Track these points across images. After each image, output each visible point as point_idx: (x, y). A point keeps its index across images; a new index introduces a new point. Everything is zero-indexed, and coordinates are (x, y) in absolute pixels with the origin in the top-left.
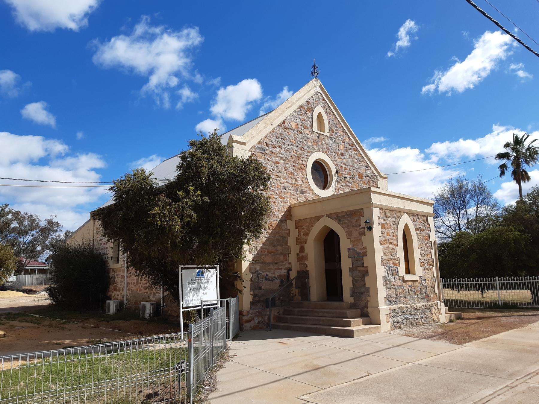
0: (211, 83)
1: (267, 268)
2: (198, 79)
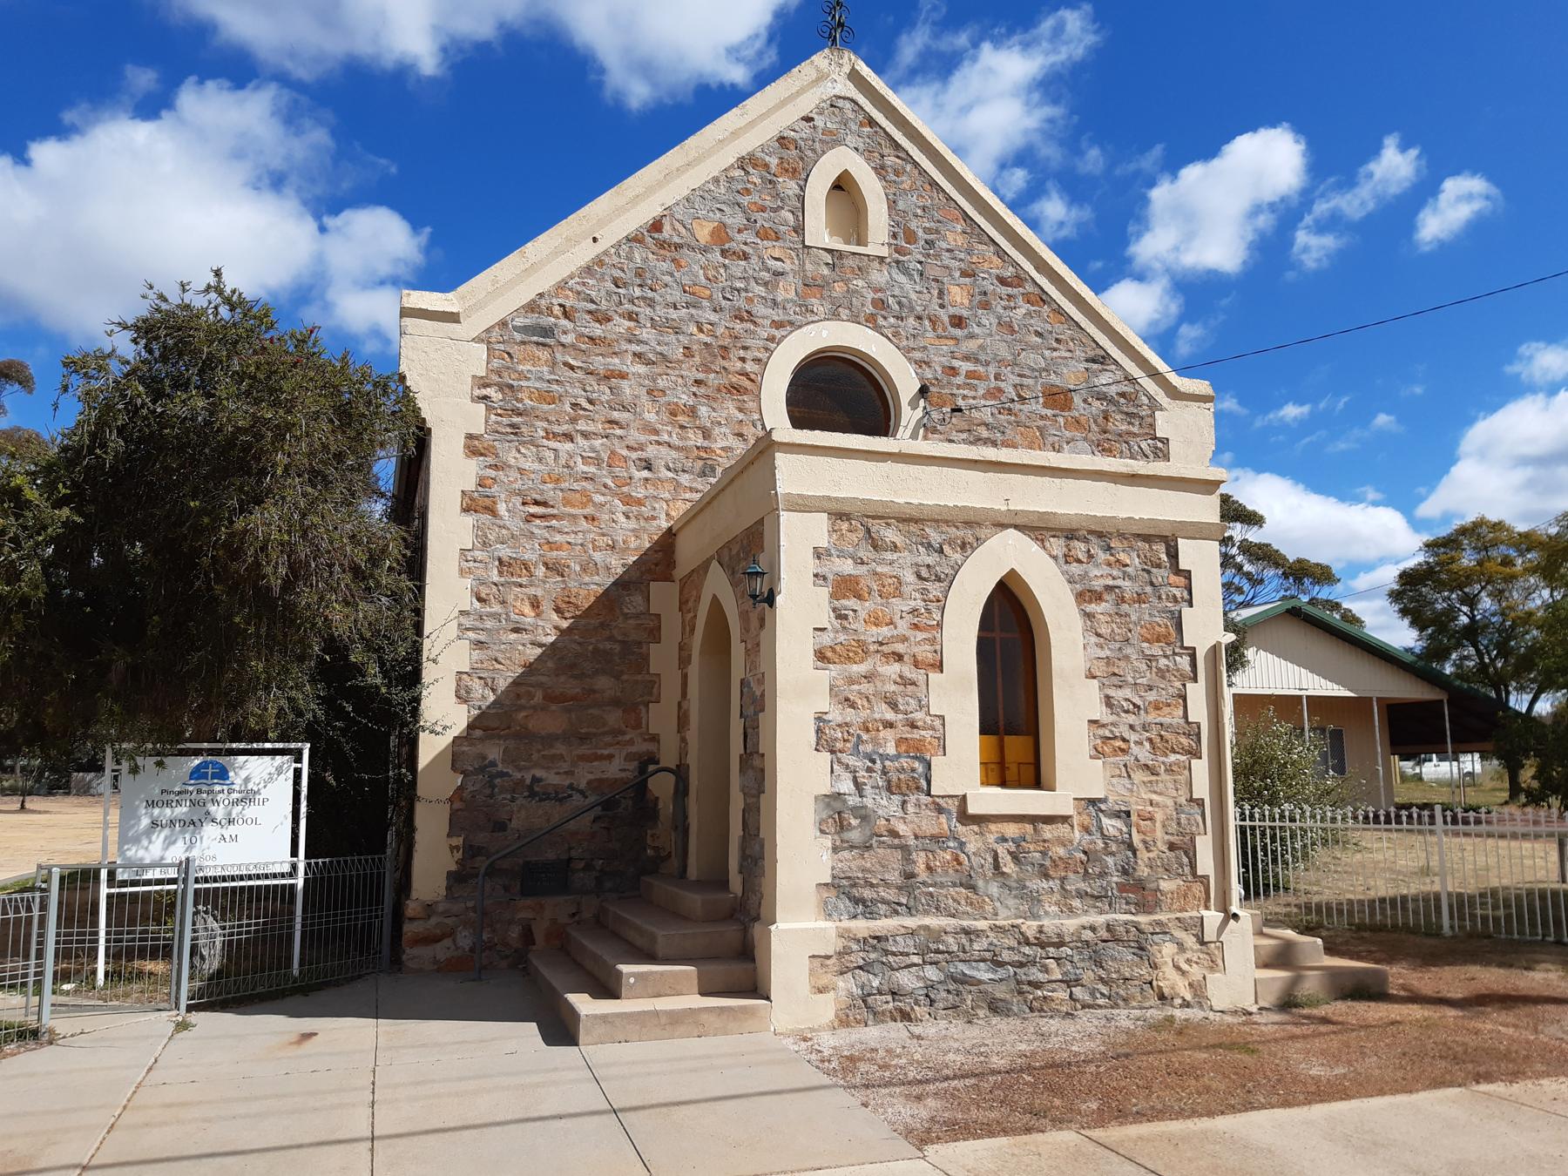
0: (1132, 167)
1: (535, 756)
2: (1093, 159)
